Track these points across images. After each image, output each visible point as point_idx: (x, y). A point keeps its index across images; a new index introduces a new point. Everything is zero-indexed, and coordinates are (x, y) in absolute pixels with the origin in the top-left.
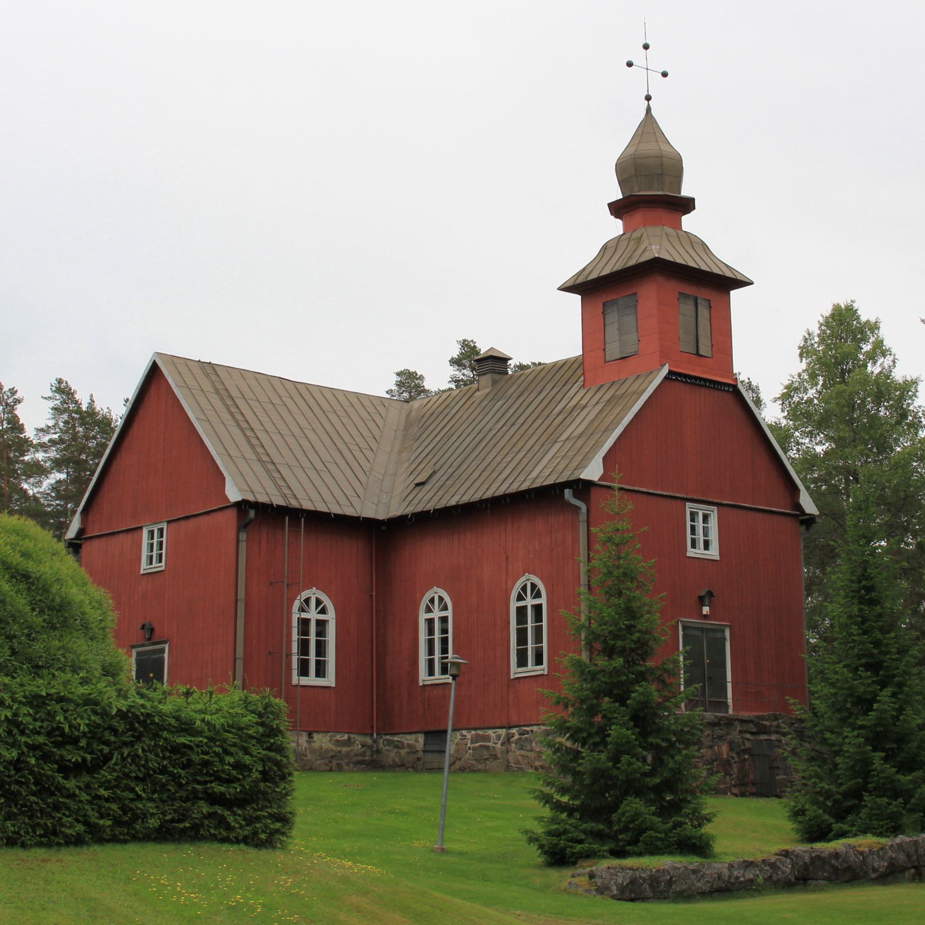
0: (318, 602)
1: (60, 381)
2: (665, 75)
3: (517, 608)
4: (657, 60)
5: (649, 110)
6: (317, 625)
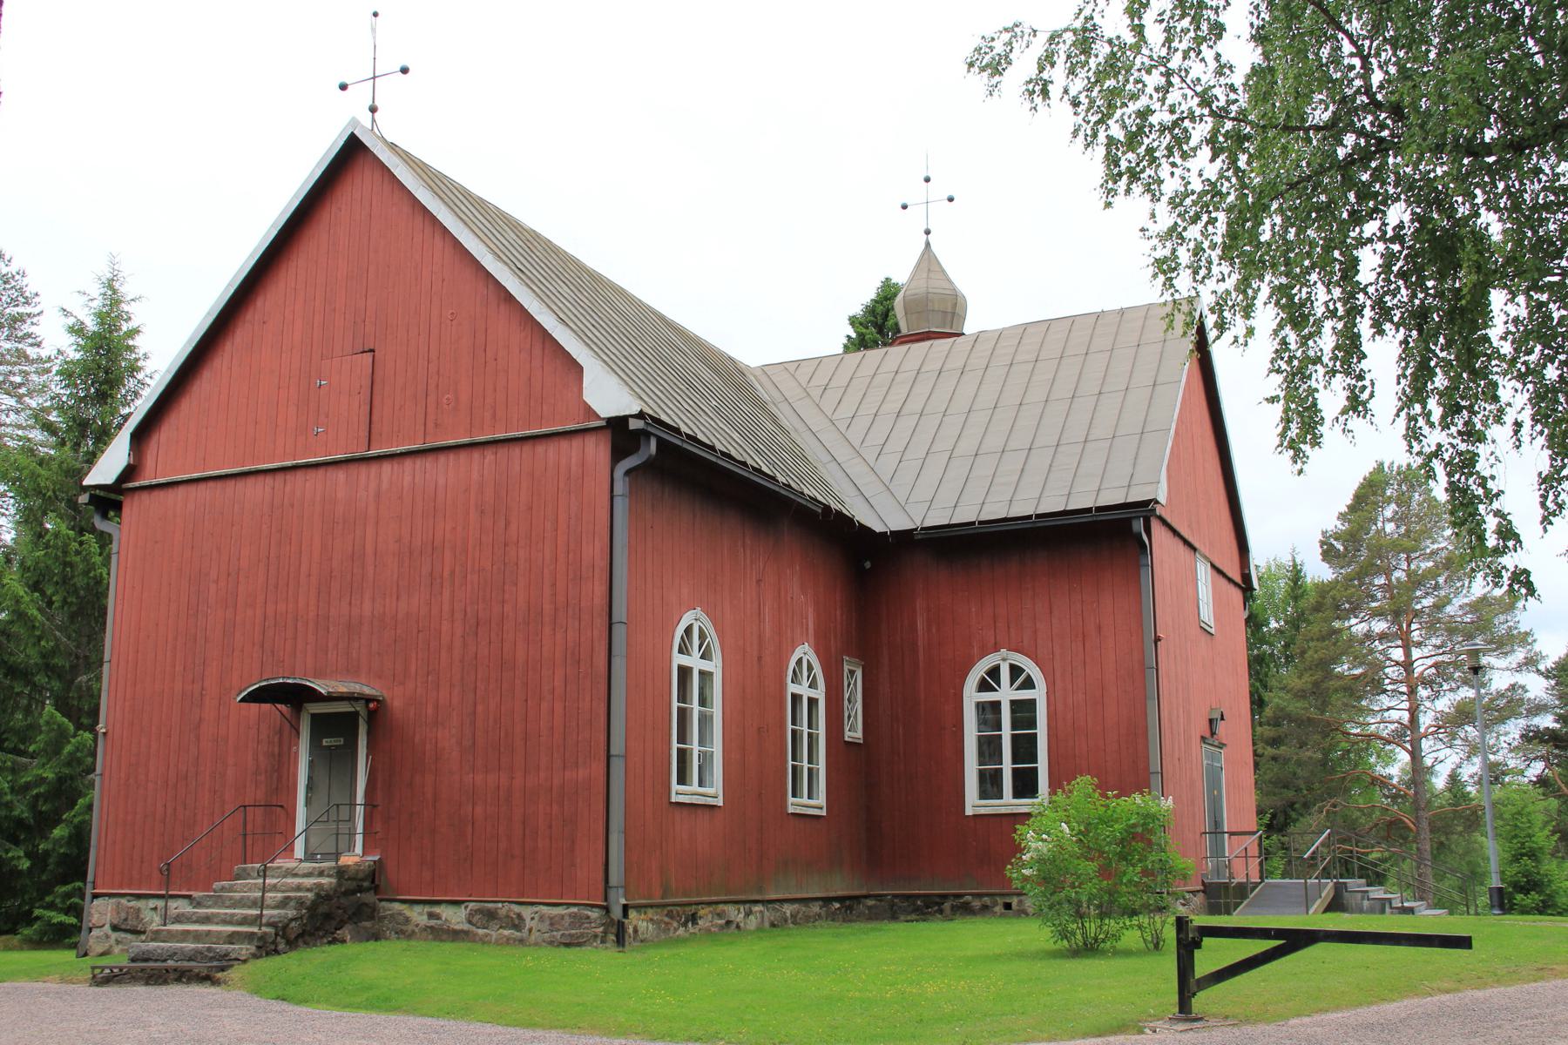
0: (1015, 671)
1: (1470, 947)
2: (376, 15)
3: (978, 704)
4: (915, 192)
5: (928, 244)
6: (1013, 711)
